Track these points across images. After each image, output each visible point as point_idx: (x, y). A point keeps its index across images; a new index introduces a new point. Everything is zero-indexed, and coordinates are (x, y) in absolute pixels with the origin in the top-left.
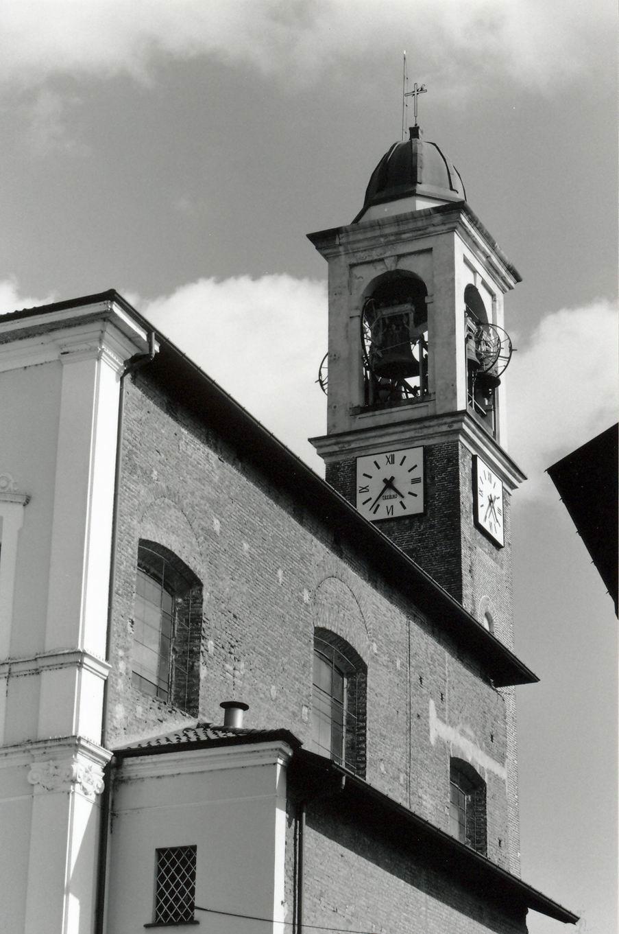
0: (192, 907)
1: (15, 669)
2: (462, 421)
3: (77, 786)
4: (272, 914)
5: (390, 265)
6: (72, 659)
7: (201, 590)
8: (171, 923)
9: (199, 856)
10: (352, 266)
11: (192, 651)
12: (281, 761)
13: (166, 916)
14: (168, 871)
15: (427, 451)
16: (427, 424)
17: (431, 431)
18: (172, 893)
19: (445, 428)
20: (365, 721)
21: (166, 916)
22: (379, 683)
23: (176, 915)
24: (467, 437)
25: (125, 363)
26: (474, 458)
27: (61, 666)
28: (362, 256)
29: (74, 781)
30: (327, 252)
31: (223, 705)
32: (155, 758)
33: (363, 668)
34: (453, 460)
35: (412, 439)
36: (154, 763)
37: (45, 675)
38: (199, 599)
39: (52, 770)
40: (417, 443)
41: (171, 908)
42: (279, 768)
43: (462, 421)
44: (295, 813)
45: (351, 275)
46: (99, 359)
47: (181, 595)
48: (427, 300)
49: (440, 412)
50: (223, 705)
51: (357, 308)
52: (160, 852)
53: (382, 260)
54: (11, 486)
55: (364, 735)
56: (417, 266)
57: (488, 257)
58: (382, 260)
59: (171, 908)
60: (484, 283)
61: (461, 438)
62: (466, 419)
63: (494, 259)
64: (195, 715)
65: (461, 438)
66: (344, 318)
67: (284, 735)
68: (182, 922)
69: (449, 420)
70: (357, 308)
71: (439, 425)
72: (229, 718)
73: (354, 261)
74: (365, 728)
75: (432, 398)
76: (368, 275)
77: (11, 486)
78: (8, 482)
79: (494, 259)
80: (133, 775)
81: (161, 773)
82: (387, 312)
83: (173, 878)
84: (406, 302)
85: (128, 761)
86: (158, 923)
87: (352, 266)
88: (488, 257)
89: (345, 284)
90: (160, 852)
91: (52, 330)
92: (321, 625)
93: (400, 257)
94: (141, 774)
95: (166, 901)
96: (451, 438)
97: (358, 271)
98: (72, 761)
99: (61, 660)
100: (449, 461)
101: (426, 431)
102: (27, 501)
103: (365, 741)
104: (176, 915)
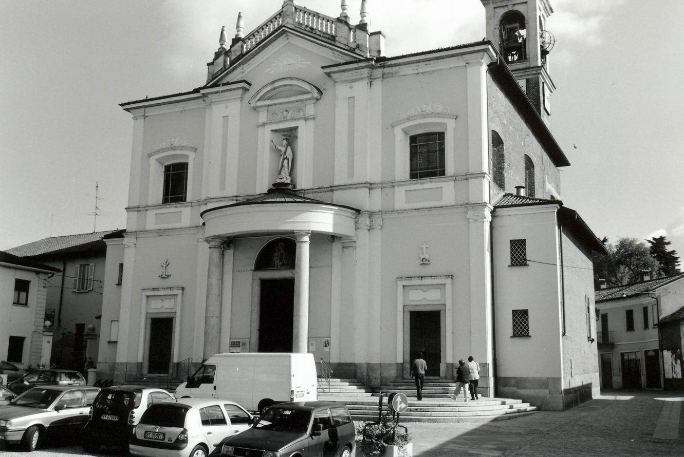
0: (525, 260)
1: (457, 178)
2: (541, 69)
3: (486, 219)
4: (334, 218)
5: (510, 8)
6: (481, 175)
7: (503, 146)
8: (517, 265)
9: (526, 240)
10: (495, 8)
11: (501, 167)
12: (556, 211)
13: (515, 262)
14: (515, 247)
15: (527, 81)
16: (528, 70)
17: (529, 73)
18: (517, 255)
19: (534, 72)
20: (534, 186)
21: (515, 262)
22: (537, 170)
23: (519, 262)
24: (542, 75)
25: (488, 66)
26: (543, 83)
27: (477, 177)
28: (499, 4)
29: (485, 218)
30: (485, 2)
31: (516, 187)
32: (508, 209)
33: (533, 167)
34: (537, 84)
35: (521, 76)
36: (508, 211)
37: (470, 180)
38: (502, 149)
39: (476, 214)
40: (524, 77)
41: (517, 260)
42: (556, 213)
43: (541, 69)
44: (559, 228)
45: (494, 11)
46: (482, 65)
47: (496, 147)
48: (526, 22)
49: (532, 66)
50: (516, 187)
51: (497, 25)
52: (511, 241)
53: (507, 6)
54: (449, 112)
55: (534, 191)
56: (521, 9)
57: (545, 4)
58: (507, 6)
59: (517, 260)
60: (543, 15)
61: (540, 76)
62: (543, 69)
63: (547, 5)
64: (504, 190)
65: (540, 76)
66: (492, 28)
67: (553, 201)
68: (521, 265)
69: (536, 69)
70: (497, 25)
71: (532, 71)
72: (518, 192)
73: (496, 6)
74: (534, 188)
75: (529, 60)
76: (502, 12)
77: (449, 112)
78: (448, 110)
79: (547, 5)
80: (499, 214)
81: (510, 214)
82: (509, 26)
83: (517, 250)
84: (516, 22)
85: (497, 210)
86: (512, 265)
87: (495, 8)
88: (545, 4)
89: (492, 15)
90: (511, 241)
91: (463, 55)
92: (525, 153)
93: (514, 5)
94: (502, 214)
95: (515, 257)
96: (537, 76)
97: (497, 10)
98: (484, 211)
99: (476, 176)
100: (536, 84)
101: (527, 73)
102: (457, 118)
103: (534, 193)
104: (519, 262)
